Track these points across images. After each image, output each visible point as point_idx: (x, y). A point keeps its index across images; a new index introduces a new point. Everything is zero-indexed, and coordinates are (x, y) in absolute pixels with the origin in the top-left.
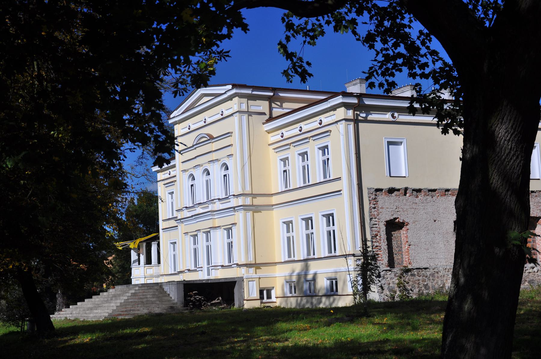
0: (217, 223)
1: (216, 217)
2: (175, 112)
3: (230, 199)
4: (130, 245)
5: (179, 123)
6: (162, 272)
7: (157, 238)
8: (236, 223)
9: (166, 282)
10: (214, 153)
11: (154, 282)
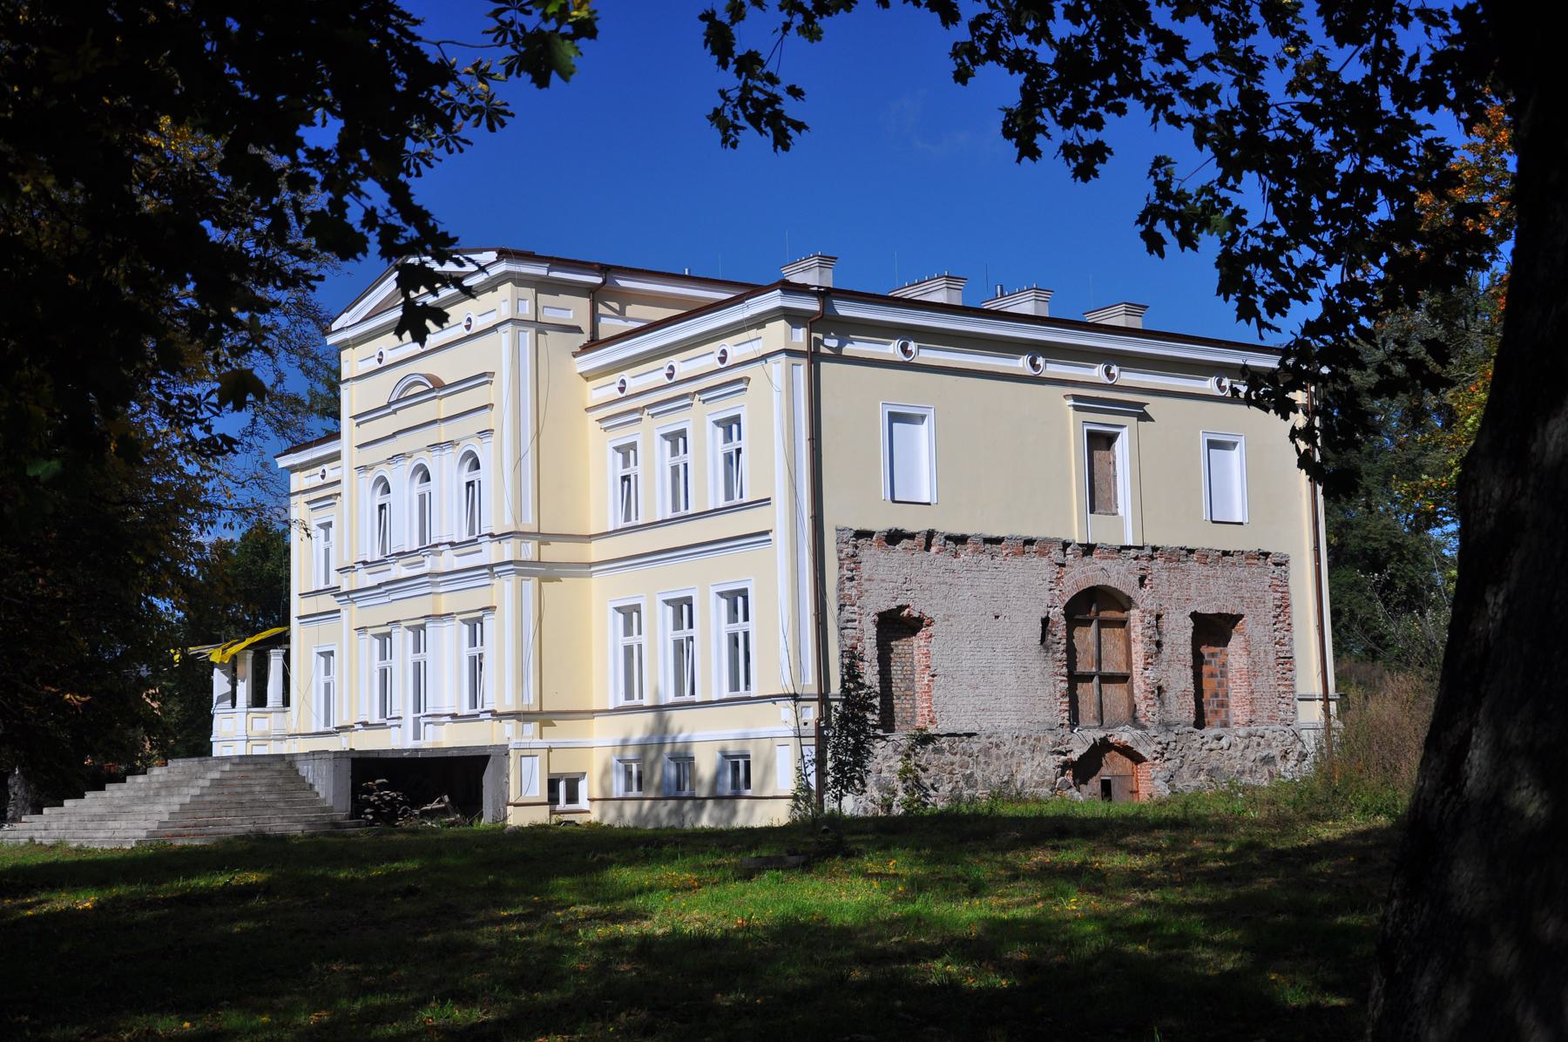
0: (444, 605)
1: (441, 590)
2: (345, 316)
5: (354, 346)
7: (283, 640)
9: (306, 754)
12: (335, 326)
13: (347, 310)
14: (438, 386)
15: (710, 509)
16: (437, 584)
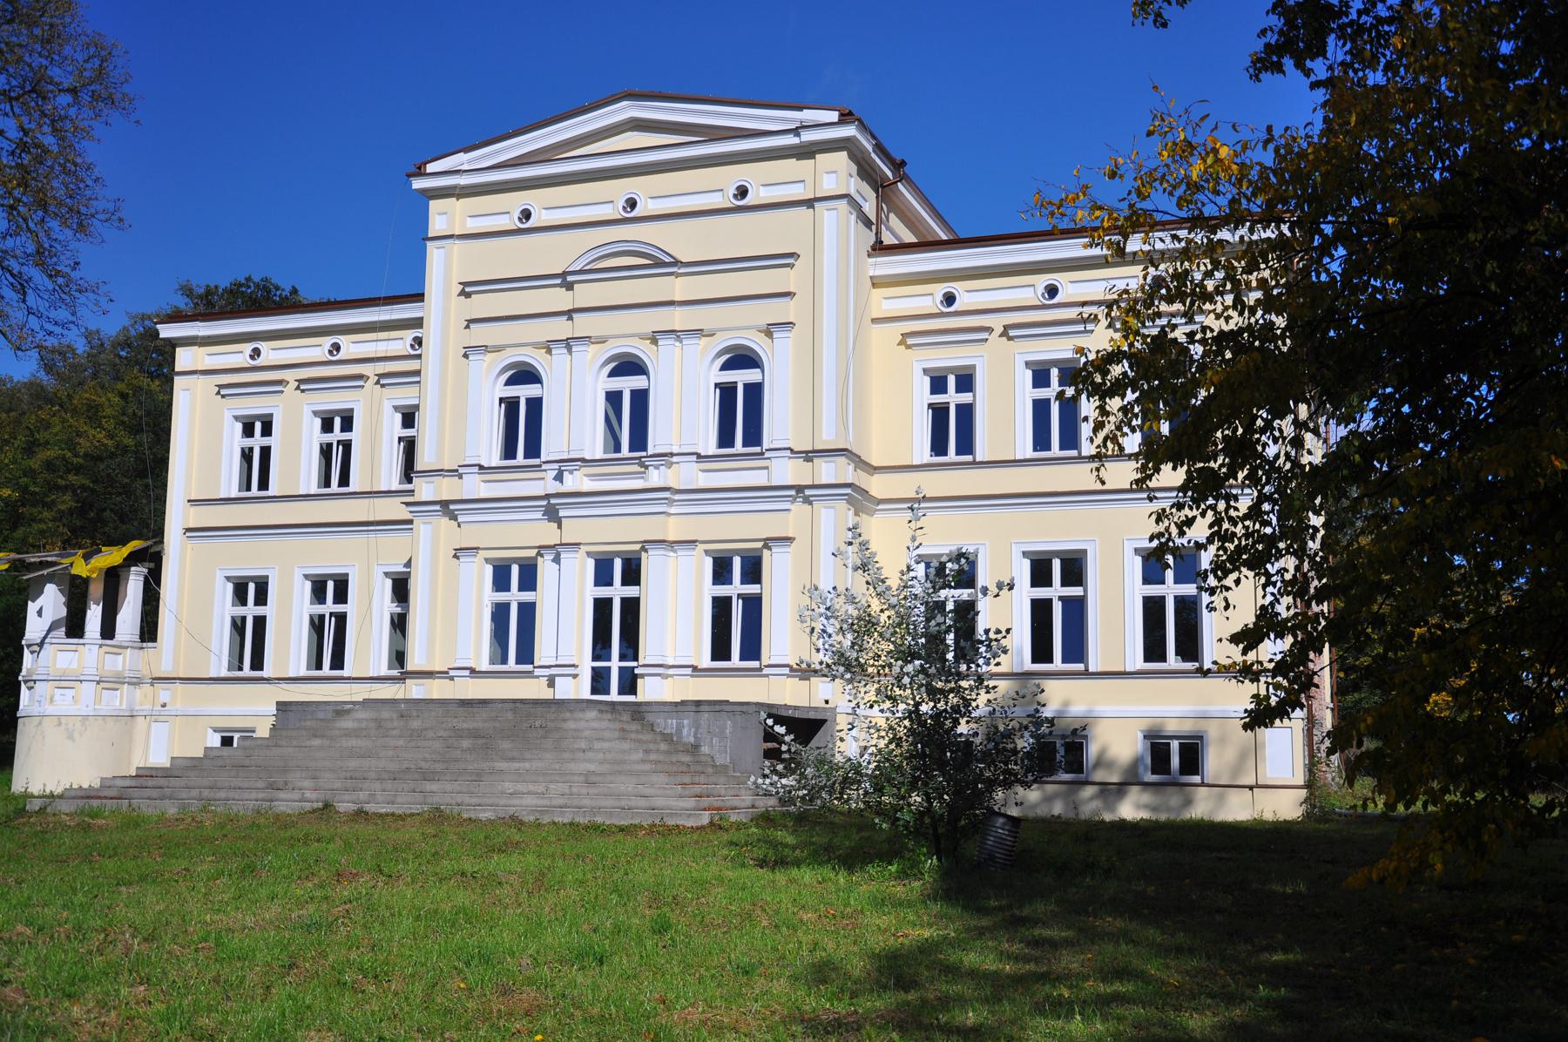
0: (673, 529)
1: (673, 510)
2: (461, 157)
3: (545, 470)
4: (72, 565)
5: (459, 197)
6: (166, 669)
7: (152, 560)
8: (794, 539)
9: (676, 704)
10: (678, 309)
11: (435, 697)
12: (431, 168)
13: (467, 150)
14: (660, 263)
15: (301, 493)
16: (670, 502)
